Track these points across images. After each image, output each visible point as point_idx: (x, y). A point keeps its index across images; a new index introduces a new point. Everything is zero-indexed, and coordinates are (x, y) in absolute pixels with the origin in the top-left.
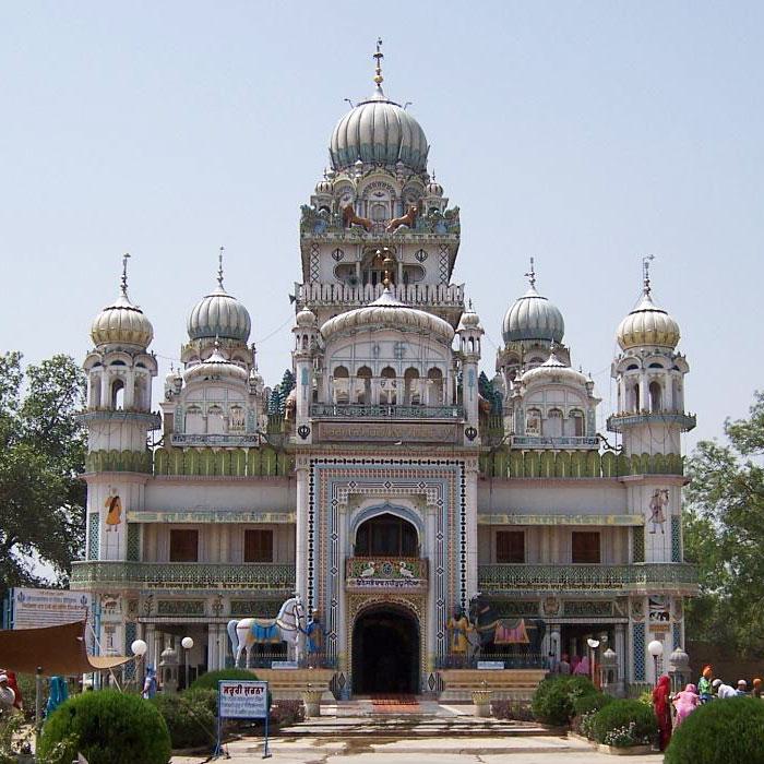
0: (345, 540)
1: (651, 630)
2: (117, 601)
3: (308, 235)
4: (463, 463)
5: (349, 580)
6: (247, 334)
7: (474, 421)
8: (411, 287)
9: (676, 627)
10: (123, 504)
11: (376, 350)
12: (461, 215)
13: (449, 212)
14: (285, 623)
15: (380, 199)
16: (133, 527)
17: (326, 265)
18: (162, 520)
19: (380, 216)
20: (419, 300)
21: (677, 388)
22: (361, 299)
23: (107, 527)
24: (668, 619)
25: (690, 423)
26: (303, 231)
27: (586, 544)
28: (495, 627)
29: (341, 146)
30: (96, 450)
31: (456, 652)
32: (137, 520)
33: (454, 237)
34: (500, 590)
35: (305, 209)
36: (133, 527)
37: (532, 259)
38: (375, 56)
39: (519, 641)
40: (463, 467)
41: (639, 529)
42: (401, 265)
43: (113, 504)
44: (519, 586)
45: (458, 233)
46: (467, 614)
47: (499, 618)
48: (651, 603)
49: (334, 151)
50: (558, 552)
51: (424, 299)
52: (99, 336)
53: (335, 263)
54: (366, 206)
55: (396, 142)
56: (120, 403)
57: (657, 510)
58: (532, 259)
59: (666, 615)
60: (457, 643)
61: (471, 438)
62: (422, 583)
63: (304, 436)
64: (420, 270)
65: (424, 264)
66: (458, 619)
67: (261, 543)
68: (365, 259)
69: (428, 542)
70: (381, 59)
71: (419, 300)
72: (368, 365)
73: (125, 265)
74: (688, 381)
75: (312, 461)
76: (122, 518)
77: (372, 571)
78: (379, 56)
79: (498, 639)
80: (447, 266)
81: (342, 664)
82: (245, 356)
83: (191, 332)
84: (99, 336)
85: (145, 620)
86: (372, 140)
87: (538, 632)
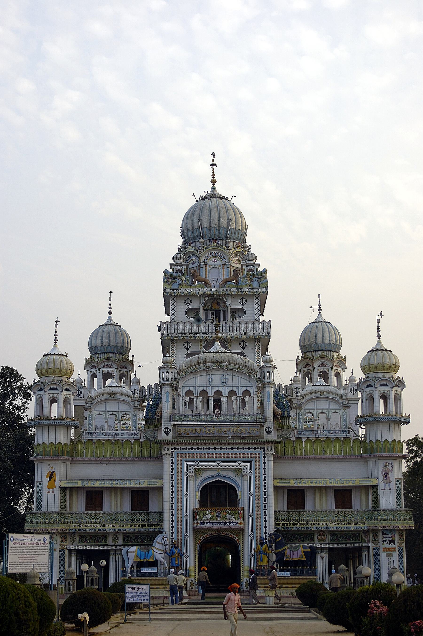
0: (193, 501)
1: (384, 551)
2: (54, 536)
3: (168, 290)
4: (264, 449)
5: (196, 522)
6: (128, 349)
7: (270, 422)
8: (236, 324)
9: (400, 548)
10: (57, 475)
11: (210, 380)
12: (268, 274)
13: (260, 272)
14: (158, 552)
15: (216, 263)
16: (63, 490)
17: (180, 309)
18: (81, 486)
19: (214, 269)
20: (241, 331)
21: (398, 398)
22: (204, 331)
23: (48, 490)
24: (394, 544)
25: (406, 421)
26: (165, 287)
27: (343, 496)
28: (285, 550)
29: (190, 227)
30: (41, 443)
31: (261, 566)
32: (66, 486)
33: (264, 289)
34: (289, 526)
35: (165, 272)
36: (63, 490)
37: (319, 295)
38: (215, 165)
39: (300, 559)
40: (264, 451)
41: (375, 488)
42: (229, 308)
43: (51, 476)
44: (301, 524)
45: (266, 287)
46: (267, 543)
47: (287, 544)
48: (383, 534)
49: (185, 231)
50: (329, 503)
51: (245, 331)
52: (41, 372)
53: (187, 308)
54: (206, 269)
55: (226, 226)
56: (54, 414)
57: (386, 476)
58: (319, 295)
59: (393, 541)
60: (261, 561)
61: (269, 433)
62: (240, 523)
63: (167, 434)
64: (242, 311)
65: (244, 307)
66: (262, 544)
67: (141, 498)
68: (206, 304)
69: (245, 499)
70: (215, 167)
71: (241, 331)
72: (205, 389)
73: (56, 327)
74: (405, 394)
75: (172, 449)
76: (57, 484)
77: (209, 516)
78: (213, 165)
79: (286, 558)
80: (259, 308)
81: (193, 574)
82: (126, 366)
83: (91, 349)
84: (41, 372)
85: (71, 548)
86: (210, 224)
87: (311, 555)
